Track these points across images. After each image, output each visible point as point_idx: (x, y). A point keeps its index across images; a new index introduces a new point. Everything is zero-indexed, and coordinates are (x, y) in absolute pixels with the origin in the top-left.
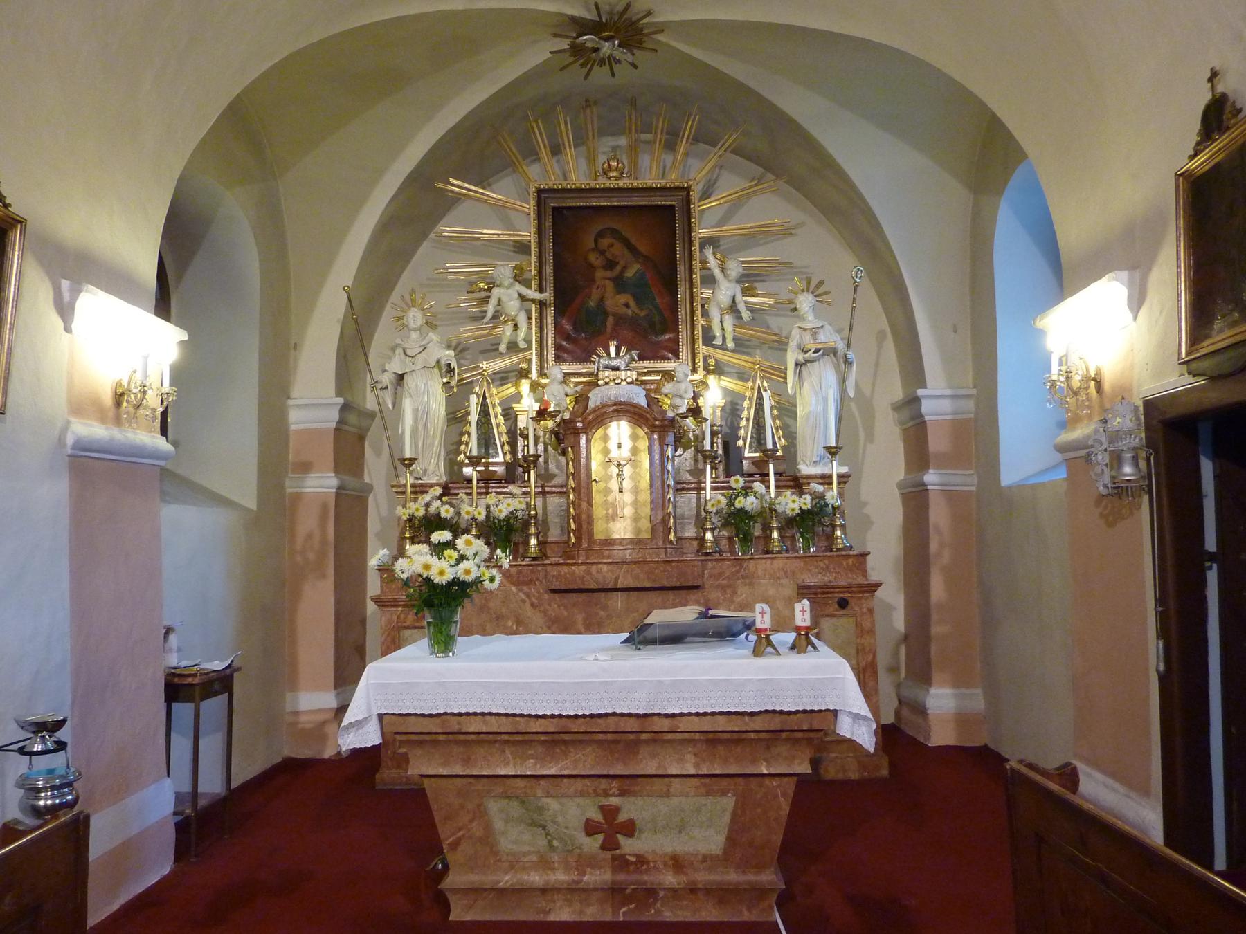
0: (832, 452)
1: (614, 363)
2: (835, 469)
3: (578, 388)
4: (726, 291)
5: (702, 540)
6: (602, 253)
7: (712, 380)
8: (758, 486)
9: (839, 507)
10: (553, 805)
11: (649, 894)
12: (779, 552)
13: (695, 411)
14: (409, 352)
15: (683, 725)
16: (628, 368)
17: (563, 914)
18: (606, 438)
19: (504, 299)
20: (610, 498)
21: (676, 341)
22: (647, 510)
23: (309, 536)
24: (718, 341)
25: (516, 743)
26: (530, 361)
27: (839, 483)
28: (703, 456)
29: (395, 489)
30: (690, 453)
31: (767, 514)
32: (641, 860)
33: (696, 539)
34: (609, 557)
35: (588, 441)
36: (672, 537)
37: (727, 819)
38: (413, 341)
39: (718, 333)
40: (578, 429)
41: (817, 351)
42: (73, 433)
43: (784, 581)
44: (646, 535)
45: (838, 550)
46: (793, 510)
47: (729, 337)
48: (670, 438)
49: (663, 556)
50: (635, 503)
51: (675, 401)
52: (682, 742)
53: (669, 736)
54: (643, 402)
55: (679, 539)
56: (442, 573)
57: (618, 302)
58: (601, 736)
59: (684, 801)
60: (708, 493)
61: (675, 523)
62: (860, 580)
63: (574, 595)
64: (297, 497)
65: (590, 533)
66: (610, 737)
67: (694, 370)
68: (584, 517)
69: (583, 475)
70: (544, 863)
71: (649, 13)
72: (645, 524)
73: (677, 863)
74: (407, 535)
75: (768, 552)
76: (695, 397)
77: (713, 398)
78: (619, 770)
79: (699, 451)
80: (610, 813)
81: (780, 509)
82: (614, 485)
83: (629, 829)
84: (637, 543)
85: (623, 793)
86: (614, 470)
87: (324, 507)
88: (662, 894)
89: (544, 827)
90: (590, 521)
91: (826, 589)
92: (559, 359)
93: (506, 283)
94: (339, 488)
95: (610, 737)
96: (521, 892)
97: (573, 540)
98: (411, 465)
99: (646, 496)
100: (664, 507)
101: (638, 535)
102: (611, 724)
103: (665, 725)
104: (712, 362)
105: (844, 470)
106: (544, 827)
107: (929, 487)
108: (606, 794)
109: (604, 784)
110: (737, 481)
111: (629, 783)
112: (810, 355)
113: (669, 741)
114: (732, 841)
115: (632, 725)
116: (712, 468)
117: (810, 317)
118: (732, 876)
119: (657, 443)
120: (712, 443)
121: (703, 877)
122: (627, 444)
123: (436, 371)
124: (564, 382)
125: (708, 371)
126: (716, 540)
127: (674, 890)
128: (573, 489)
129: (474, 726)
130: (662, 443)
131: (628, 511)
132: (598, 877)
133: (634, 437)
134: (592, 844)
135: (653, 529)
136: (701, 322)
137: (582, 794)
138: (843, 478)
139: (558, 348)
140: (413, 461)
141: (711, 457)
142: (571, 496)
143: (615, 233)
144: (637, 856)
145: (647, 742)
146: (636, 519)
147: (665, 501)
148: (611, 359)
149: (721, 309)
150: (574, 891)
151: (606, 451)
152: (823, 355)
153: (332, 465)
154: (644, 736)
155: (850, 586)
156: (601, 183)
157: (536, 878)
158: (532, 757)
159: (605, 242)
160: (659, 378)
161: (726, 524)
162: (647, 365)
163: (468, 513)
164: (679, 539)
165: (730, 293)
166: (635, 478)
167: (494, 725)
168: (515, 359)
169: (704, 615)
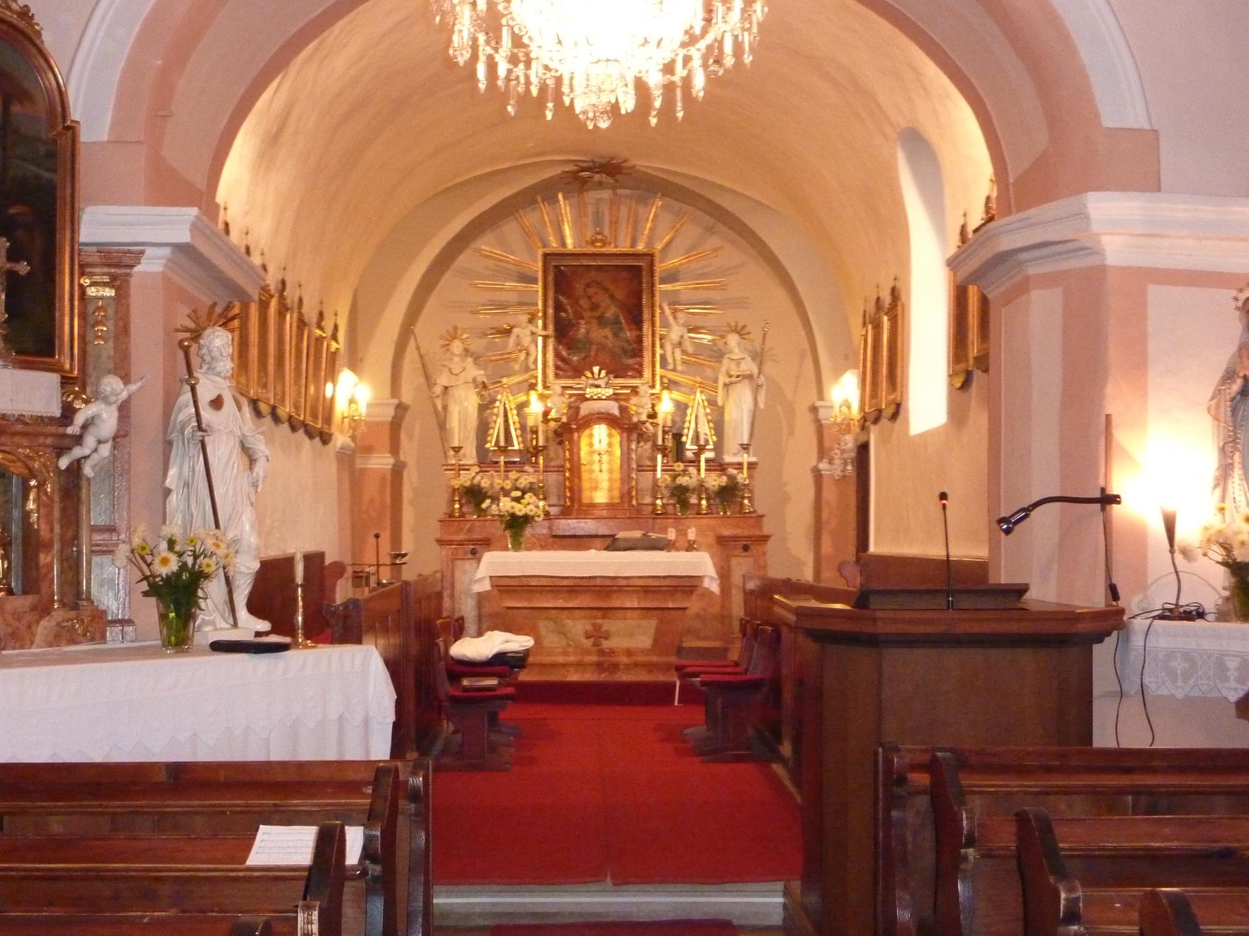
0: (745, 447)
1: (597, 382)
2: (745, 458)
3: (572, 400)
4: (676, 333)
5: (654, 505)
6: (590, 298)
7: (665, 394)
8: (692, 470)
9: (747, 485)
10: (569, 622)
11: (615, 667)
12: (705, 514)
13: (653, 416)
14: (454, 372)
15: (633, 582)
16: (607, 385)
17: (574, 677)
18: (591, 436)
19: (521, 335)
20: (594, 476)
21: (641, 365)
22: (617, 485)
23: (372, 501)
24: (671, 367)
25: (552, 591)
26: (536, 377)
27: (748, 468)
28: (656, 448)
29: (445, 467)
30: (648, 446)
31: (701, 488)
32: (612, 652)
33: (651, 505)
34: (592, 515)
35: (579, 437)
36: (634, 502)
37: (653, 631)
38: (456, 363)
39: (670, 360)
40: (571, 429)
41: (738, 376)
42: (1179, 546)
43: (709, 533)
44: (617, 501)
45: (745, 513)
46: (714, 486)
47: (679, 362)
48: (634, 436)
49: (628, 515)
50: (610, 480)
51: (639, 409)
52: (634, 591)
53: (626, 588)
54: (616, 412)
55: (639, 504)
56: (520, 510)
57: (601, 335)
58: (593, 588)
59: (632, 621)
60: (659, 474)
61: (637, 493)
62: (757, 533)
63: (569, 539)
64: (363, 472)
65: (580, 499)
66: (597, 589)
67: (653, 387)
68: (576, 488)
69: (576, 459)
70: (565, 653)
71: (625, 161)
72: (616, 494)
73: (629, 653)
74: (457, 498)
75: (698, 514)
76: (653, 406)
77: (666, 408)
78: (602, 605)
79: (655, 446)
80: (597, 628)
81: (707, 485)
82: (596, 467)
83: (607, 636)
84: (610, 506)
85: (603, 617)
86: (596, 458)
87: (383, 479)
88: (622, 667)
89: (565, 635)
90: (580, 491)
91: (735, 538)
92: (557, 376)
93: (524, 325)
94: (394, 465)
95: (597, 589)
96: (553, 666)
97: (568, 504)
98: (458, 451)
99: (617, 475)
100: (629, 483)
101: (612, 500)
102: (598, 582)
103: (624, 583)
104: (665, 380)
105: (753, 459)
106: (565, 635)
107: (823, 472)
108: (596, 618)
109: (595, 613)
110: (679, 466)
111: (607, 611)
112: (734, 379)
113: (626, 591)
114: (656, 641)
115: (609, 583)
116: (663, 457)
117: (736, 350)
118: (654, 659)
119: (625, 439)
120: (664, 439)
121: (641, 659)
122: (605, 441)
123: (472, 385)
124: (562, 395)
125: (664, 388)
126: (664, 506)
127: (627, 665)
128: (569, 469)
129: (534, 582)
130: (629, 441)
131: (605, 485)
132: (594, 658)
133: (610, 436)
134: (588, 643)
135: (622, 497)
136: (659, 351)
137: (585, 618)
138: (752, 466)
139: (557, 367)
140: (460, 448)
141: (663, 450)
142: (567, 474)
143: (598, 284)
144: (610, 649)
145: (615, 591)
146: (611, 490)
147: (630, 478)
148: (596, 379)
149: (674, 345)
150: (580, 665)
151: (591, 445)
152: (743, 378)
153: (388, 449)
154: (614, 588)
155: (751, 537)
156: (591, 250)
157: (561, 659)
158: (562, 599)
159: (592, 291)
160: (629, 391)
161: (672, 495)
162: (620, 381)
163: (498, 484)
164: (639, 504)
165: (679, 333)
166: (610, 462)
167: (544, 582)
168: (526, 376)
169: (644, 535)
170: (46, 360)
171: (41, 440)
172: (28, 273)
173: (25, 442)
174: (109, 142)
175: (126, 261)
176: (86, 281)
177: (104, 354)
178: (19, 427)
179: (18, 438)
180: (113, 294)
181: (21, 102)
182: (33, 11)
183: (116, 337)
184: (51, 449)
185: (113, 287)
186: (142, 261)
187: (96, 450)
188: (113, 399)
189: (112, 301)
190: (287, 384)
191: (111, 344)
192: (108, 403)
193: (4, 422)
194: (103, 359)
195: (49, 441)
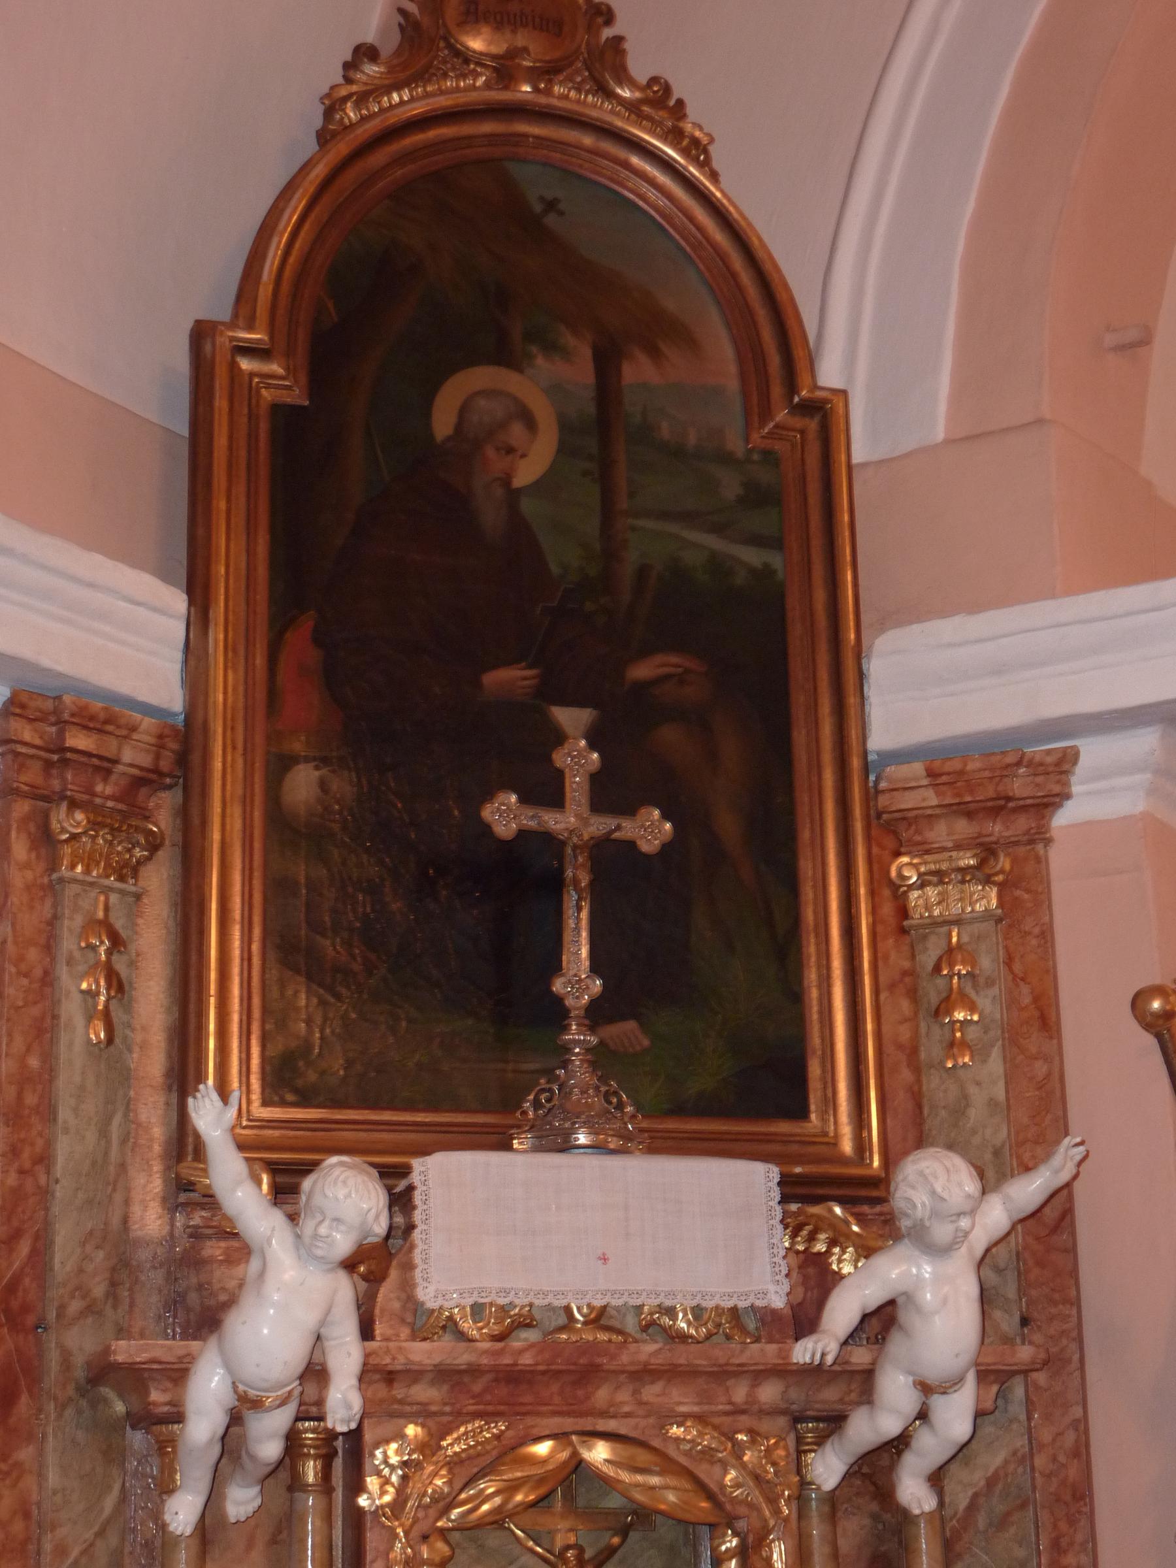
170: (784, 1127)
171: (740, 1393)
172: (666, 848)
173: (682, 1399)
174: (948, 442)
175: (1020, 786)
176: (906, 868)
177: (978, 1097)
178: (649, 1350)
179: (657, 1387)
180: (994, 903)
181: (655, 353)
182: (627, 46)
183: (1013, 1039)
184: (782, 1421)
185: (988, 881)
186: (1076, 789)
187: (923, 1415)
188: (942, 1232)
189: (989, 926)
190: (126, 768)
191: (995, 1064)
192: (938, 1251)
193: (602, 1336)
194: (975, 1114)
195: (769, 1393)
